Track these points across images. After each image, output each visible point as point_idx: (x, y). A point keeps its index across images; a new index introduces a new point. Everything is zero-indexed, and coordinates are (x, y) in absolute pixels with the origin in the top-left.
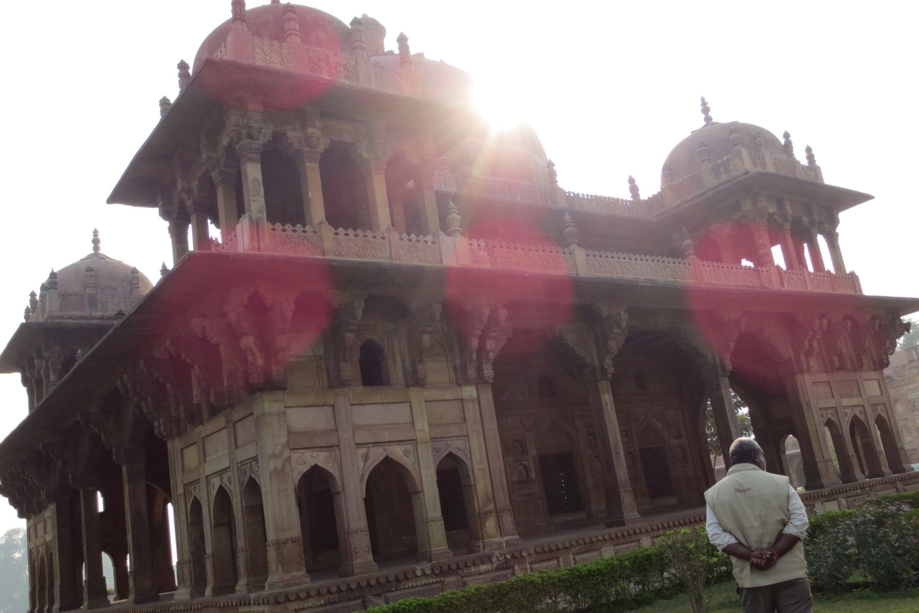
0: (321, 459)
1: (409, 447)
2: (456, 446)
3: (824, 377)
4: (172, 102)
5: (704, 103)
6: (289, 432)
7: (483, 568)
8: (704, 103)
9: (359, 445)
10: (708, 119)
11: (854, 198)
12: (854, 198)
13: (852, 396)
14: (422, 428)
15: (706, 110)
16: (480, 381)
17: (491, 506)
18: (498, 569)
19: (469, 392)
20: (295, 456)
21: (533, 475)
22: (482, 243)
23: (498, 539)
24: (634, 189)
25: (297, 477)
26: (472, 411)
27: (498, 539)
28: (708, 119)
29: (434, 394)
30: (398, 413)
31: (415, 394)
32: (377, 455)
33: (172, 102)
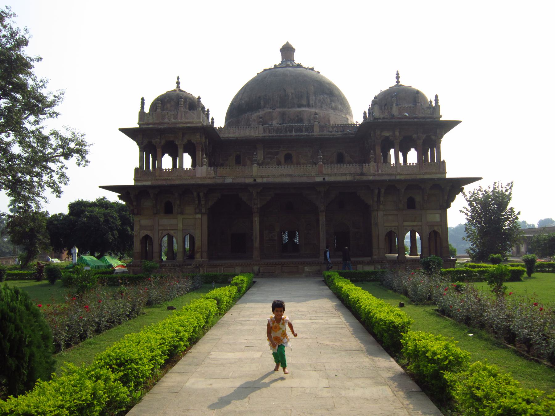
0: (149, 233)
4: (441, 119)
5: (398, 74)
7: (189, 267)
8: (398, 74)
9: (159, 230)
10: (398, 82)
11: (128, 132)
12: (128, 132)
13: (414, 221)
14: (180, 226)
15: (398, 77)
16: (202, 214)
17: (200, 250)
18: (194, 268)
19: (199, 216)
20: (142, 232)
22: (212, 168)
23: (200, 260)
24: (365, 117)
25: (141, 237)
27: (200, 260)
28: (398, 82)
32: (389, 230)
33: (441, 119)
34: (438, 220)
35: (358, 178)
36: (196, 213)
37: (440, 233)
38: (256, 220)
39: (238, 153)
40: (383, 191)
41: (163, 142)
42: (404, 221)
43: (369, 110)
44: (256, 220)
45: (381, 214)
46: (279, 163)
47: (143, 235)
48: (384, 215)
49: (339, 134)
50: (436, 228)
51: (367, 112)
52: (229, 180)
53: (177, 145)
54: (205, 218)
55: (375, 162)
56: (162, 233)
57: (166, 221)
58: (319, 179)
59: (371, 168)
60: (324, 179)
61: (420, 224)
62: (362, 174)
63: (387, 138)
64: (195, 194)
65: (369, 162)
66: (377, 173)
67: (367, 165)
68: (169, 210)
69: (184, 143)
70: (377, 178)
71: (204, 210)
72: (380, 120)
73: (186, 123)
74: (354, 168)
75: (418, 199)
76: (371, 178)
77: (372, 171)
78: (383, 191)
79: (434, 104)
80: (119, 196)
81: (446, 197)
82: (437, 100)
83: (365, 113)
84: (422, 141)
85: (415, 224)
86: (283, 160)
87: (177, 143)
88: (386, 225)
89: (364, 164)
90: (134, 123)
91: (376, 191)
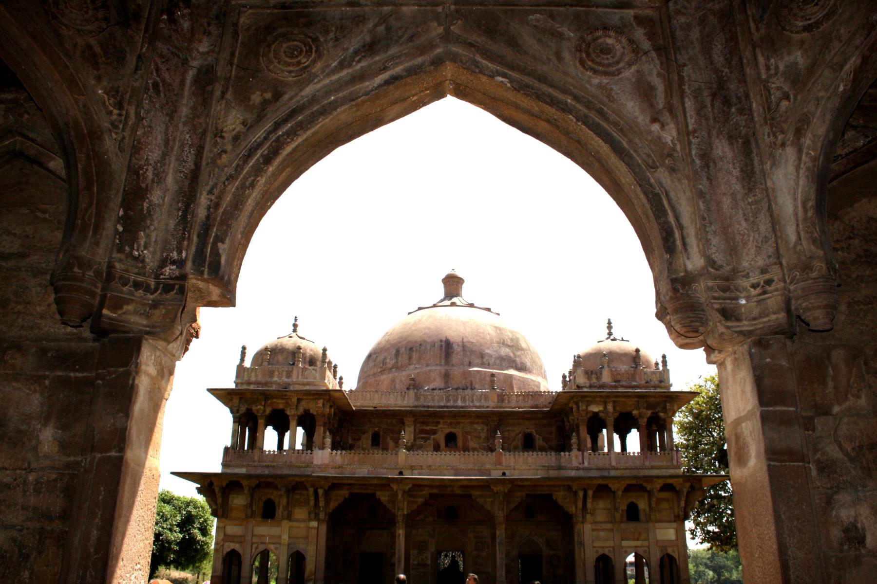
0: (236, 547)
1: (278, 546)
2: (301, 547)
3: (609, 526)
5: (609, 323)
6: (225, 535)
8: (609, 323)
13: (638, 540)
16: (316, 517)
19: (314, 524)
20: (227, 544)
21: (429, 562)
25: (225, 553)
26: (314, 532)
29: (295, 524)
30: (274, 531)
31: (286, 524)
34: (673, 537)
35: (553, 473)
36: (310, 520)
37: (677, 557)
38: (401, 532)
39: (376, 429)
40: (590, 493)
41: (268, 410)
42: (622, 539)
43: (570, 373)
44: (401, 532)
45: (588, 527)
46: (437, 448)
47: (229, 550)
48: (593, 530)
49: (524, 407)
50: (670, 551)
51: (567, 375)
52: (363, 471)
53: (288, 416)
54: (324, 528)
55: (579, 450)
56: (257, 548)
57: (265, 530)
58: (496, 474)
59: (574, 458)
60: (504, 474)
61: (646, 543)
62: (560, 468)
63: (596, 414)
64: (311, 490)
65: (570, 450)
66: (581, 466)
67: (567, 453)
68: (269, 512)
69: (299, 413)
70: (581, 473)
71: (322, 516)
72: (585, 390)
73: (304, 384)
74: (549, 459)
75: (642, 505)
76: (573, 473)
77: (575, 463)
78: (590, 493)
79: (661, 368)
80: (197, 488)
81: (683, 504)
82: (664, 362)
83: (564, 377)
84: (645, 420)
85: (639, 543)
86: (442, 443)
87: (288, 413)
88: (595, 545)
89: (562, 453)
90: (229, 383)
91: (581, 494)
